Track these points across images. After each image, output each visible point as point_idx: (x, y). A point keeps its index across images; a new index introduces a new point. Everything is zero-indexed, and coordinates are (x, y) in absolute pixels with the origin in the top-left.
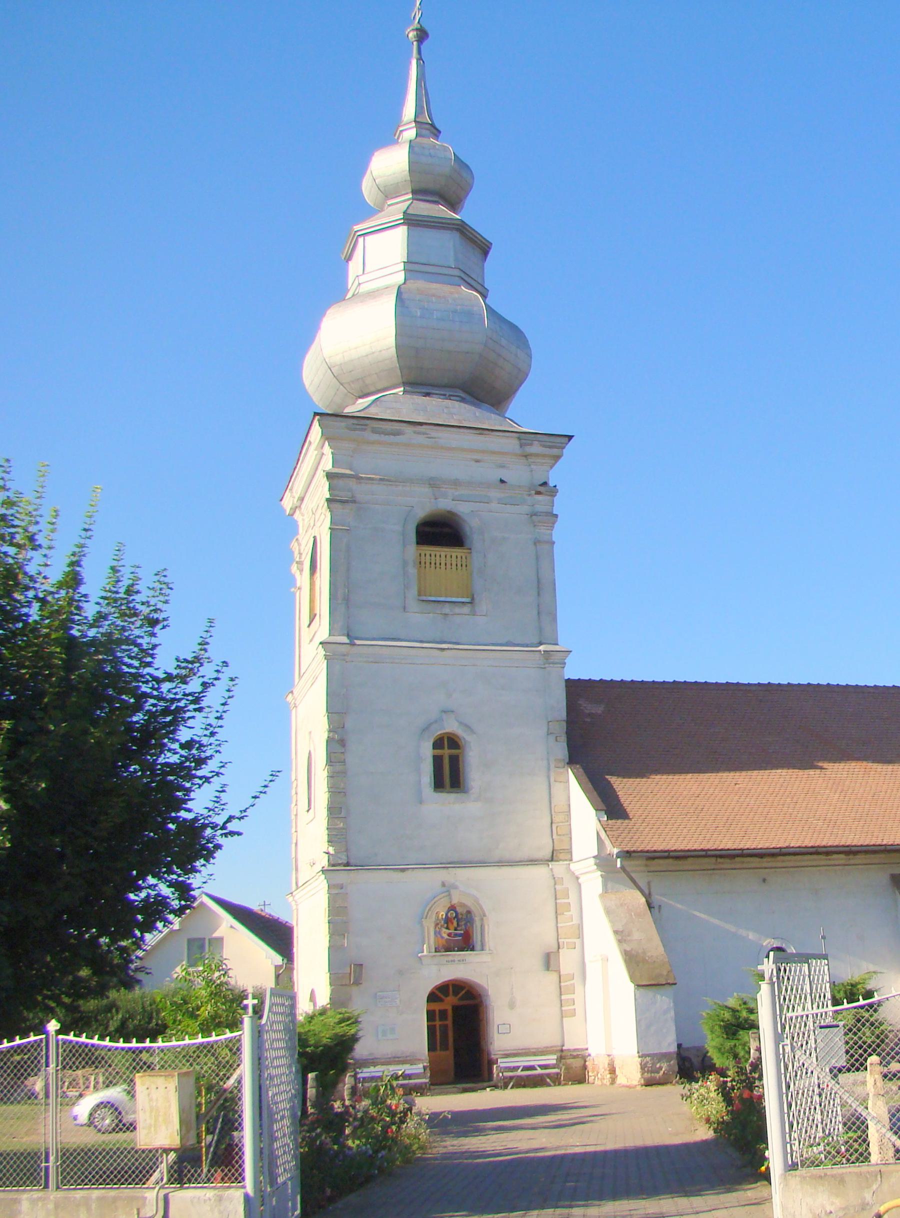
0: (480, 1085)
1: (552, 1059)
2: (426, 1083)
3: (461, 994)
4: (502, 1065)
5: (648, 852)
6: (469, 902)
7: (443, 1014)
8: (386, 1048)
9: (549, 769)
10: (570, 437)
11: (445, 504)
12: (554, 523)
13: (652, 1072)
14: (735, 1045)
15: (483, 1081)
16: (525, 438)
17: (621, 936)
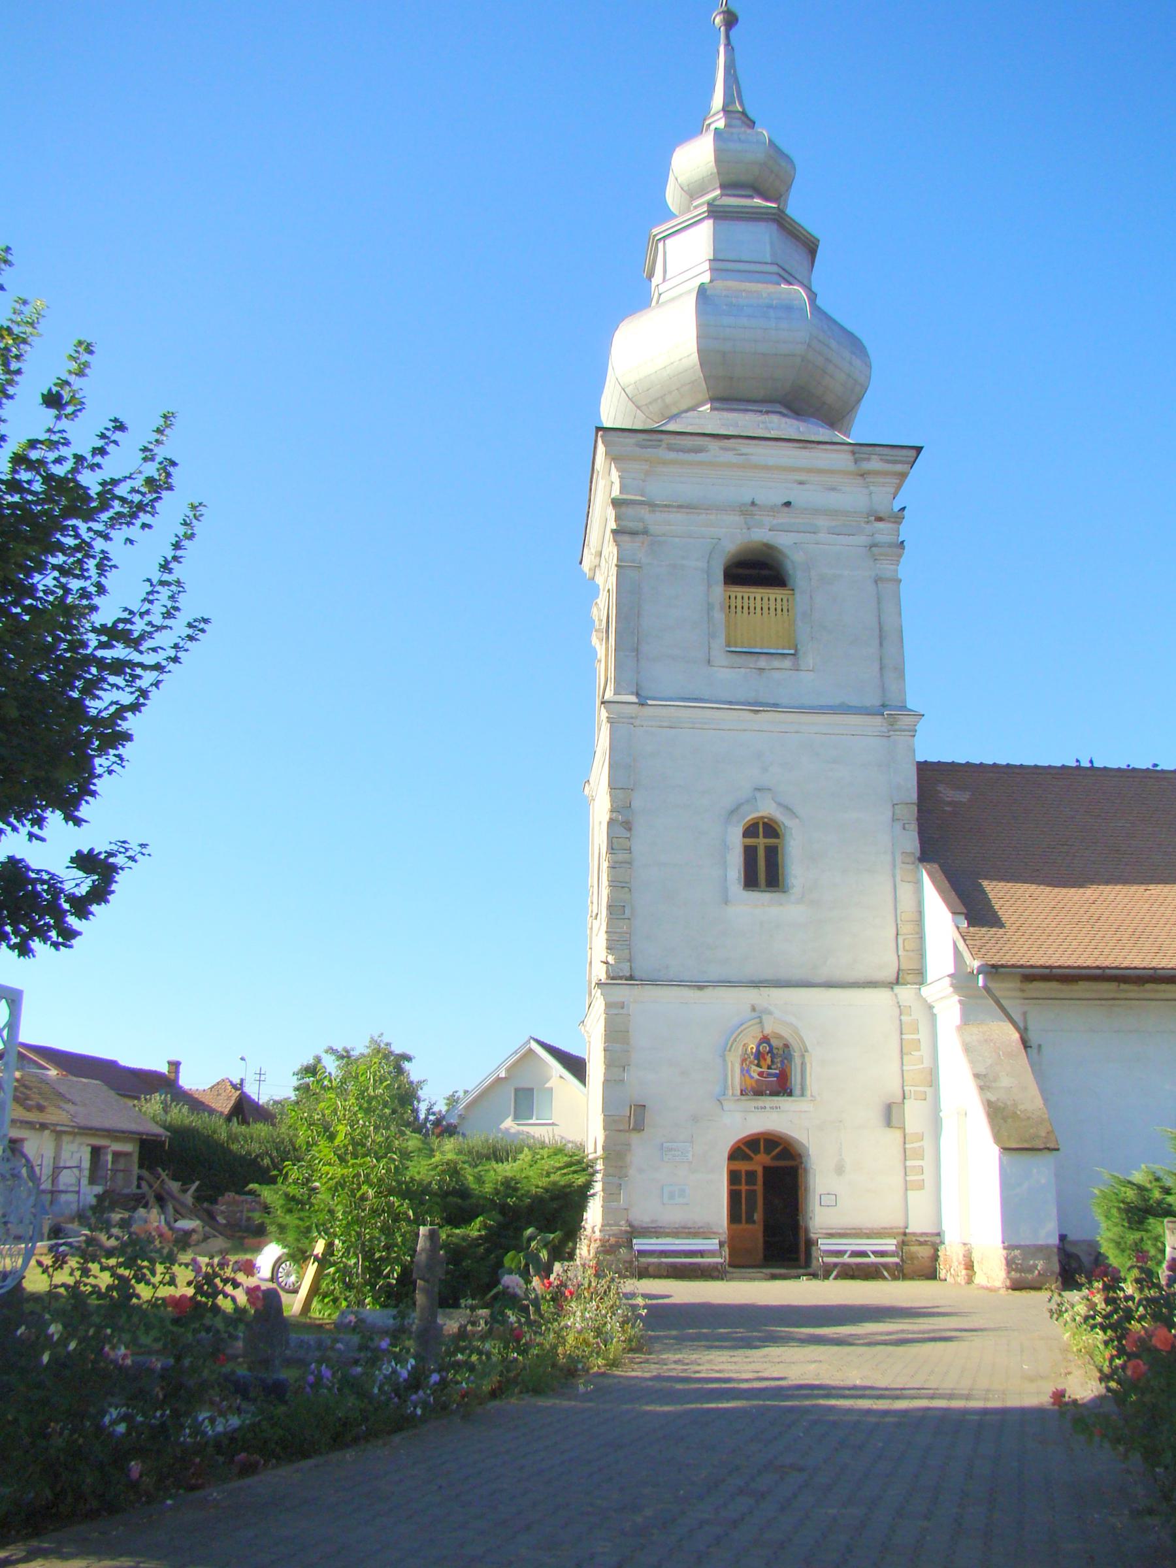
0: (793, 1272)
1: (890, 1244)
2: (722, 1264)
3: (775, 1153)
4: (823, 1248)
5: (1022, 966)
6: (785, 1033)
7: (751, 1175)
8: (672, 1216)
9: (894, 866)
10: (919, 450)
11: (760, 535)
12: (900, 556)
13: (1021, 1271)
14: (1142, 1240)
15: (800, 1267)
16: (861, 450)
17: (984, 1081)
